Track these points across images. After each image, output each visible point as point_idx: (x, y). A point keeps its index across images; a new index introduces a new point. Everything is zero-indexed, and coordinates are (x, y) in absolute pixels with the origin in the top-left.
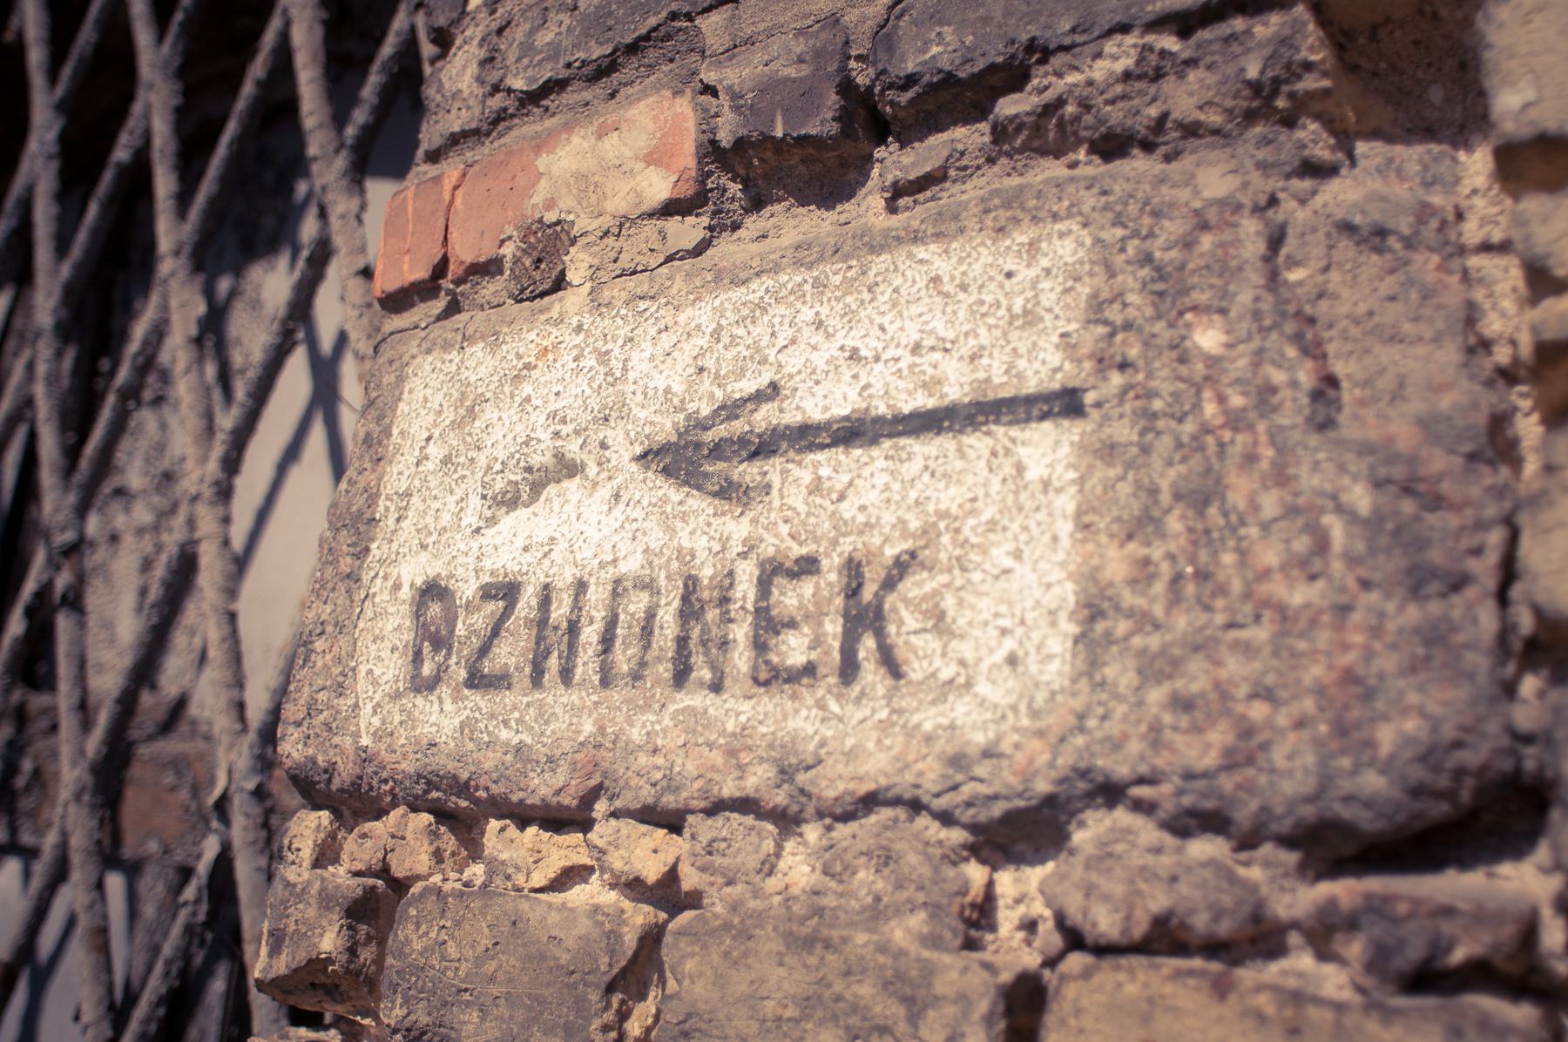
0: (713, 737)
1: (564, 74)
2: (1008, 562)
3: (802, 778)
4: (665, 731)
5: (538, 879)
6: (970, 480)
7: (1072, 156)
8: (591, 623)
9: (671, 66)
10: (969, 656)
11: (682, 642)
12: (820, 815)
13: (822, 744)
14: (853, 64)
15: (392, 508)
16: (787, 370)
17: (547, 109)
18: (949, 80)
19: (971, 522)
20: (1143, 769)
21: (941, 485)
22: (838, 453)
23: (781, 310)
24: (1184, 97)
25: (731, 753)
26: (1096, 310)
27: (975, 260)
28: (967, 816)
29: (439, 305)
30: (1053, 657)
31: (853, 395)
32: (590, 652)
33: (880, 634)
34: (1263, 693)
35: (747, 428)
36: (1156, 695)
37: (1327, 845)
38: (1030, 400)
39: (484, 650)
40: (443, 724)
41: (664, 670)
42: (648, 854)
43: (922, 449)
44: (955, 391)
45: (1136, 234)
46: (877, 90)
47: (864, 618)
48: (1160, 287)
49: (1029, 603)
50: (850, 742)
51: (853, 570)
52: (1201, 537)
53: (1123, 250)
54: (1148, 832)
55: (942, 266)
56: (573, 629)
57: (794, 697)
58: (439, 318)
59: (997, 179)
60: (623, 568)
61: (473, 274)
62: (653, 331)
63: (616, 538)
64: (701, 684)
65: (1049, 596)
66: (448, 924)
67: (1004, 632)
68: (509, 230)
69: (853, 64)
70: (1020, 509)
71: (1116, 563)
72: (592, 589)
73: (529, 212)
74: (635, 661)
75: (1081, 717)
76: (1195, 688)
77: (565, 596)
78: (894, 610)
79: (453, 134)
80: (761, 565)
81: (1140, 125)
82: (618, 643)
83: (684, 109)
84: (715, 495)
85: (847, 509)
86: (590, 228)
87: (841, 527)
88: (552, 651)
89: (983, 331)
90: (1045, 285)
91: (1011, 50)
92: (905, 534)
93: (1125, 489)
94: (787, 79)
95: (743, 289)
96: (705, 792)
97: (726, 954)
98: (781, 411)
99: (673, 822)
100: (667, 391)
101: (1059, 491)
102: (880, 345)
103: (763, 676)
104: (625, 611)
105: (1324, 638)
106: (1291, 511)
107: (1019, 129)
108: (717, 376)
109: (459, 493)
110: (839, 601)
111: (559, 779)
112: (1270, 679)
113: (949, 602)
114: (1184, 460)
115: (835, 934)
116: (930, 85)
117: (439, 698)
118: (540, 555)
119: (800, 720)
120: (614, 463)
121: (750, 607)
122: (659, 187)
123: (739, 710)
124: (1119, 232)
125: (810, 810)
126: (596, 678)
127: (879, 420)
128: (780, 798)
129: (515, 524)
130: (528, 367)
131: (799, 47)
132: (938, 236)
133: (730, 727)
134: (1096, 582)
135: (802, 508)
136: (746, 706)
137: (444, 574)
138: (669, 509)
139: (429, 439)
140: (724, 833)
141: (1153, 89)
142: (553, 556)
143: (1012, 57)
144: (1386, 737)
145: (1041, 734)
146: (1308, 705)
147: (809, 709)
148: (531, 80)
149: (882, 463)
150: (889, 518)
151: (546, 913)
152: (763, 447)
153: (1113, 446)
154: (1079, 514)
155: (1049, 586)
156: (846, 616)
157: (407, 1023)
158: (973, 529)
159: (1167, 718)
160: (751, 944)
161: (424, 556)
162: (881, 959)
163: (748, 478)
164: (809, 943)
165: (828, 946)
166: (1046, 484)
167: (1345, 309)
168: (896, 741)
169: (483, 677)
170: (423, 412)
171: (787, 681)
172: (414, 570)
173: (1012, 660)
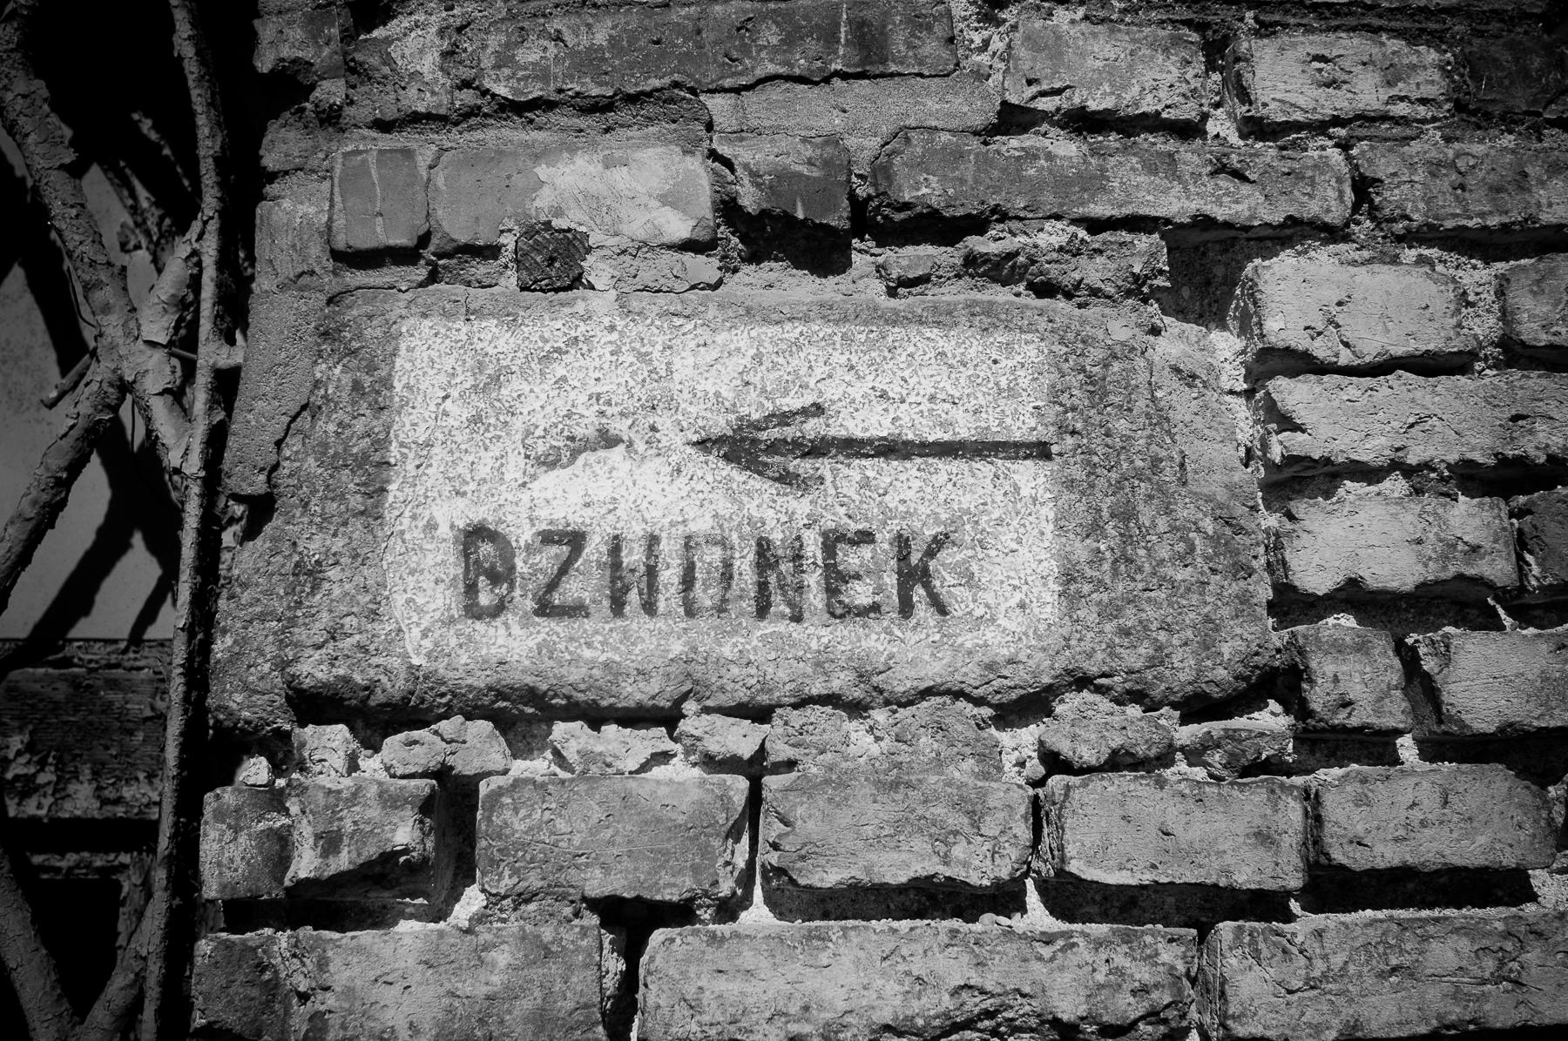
0: (801, 653)
1: (554, 97)
2: (1014, 546)
3: (875, 680)
4: (755, 649)
6: (981, 491)
7: (1016, 289)
9: (674, 126)
10: (991, 602)
11: (763, 586)
13: (891, 657)
14: (854, 179)
15: (411, 455)
17: (531, 121)
18: (935, 214)
19: (985, 518)
20: (1105, 669)
21: (960, 492)
22: (880, 462)
23: (814, 350)
24: (1093, 271)
25: (818, 664)
26: (1055, 395)
27: (966, 344)
28: (996, 699)
29: (421, 272)
30: (1047, 603)
31: (887, 422)
32: (673, 590)
33: (927, 586)
34: (1166, 627)
35: (799, 434)
36: (1109, 627)
37: (1196, 707)
38: (1017, 446)
39: (552, 586)
40: (513, 646)
41: (748, 605)
42: (740, 739)
43: (945, 468)
44: (964, 429)
45: (1074, 352)
46: (874, 204)
47: (913, 575)
48: (1091, 388)
49: (1029, 571)
50: (911, 655)
51: (902, 543)
52: (1126, 538)
53: (1067, 360)
54: (1104, 704)
55: (948, 347)
56: (652, 572)
57: (864, 626)
58: (422, 285)
59: (954, 293)
60: (693, 527)
61: (464, 253)
62: (692, 344)
63: (682, 504)
64: (783, 616)
66: (553, 806)
67: (1015, 588)
68: (510, 224)
69: (854, 179)
70: (1017, 513)
71: (1081, 551)
73: (533, 213)
74: (718, 597)
76: (1129, 624)
77: (636, 546)
79: (415, 113)
80: (825, 534)
81: (1067, 281)
82: (698, 585)
83: (697, 168)
85: (891, 500)
86: (608, 243)
87: (887, 514)
88: (628, 587)
89: (979, 395)
90: (1021, 373)
92: (937, 521)
93: (1081, 507)
94: (800, 175)
96: (793, 693)
97: (830, 800)
99: (760, 714)
100: (717, 395)
101: (1042, 504)
103: (839, 611)
104: (700, 560)
106: (1173, 529)
107: (984, 262)
109: (496, 450)
110: (893, 563)
111: (654, 686)
112: (1169, 620)
113: (975, 568)
114: (1114, 494)
115: (913, 778)
116: (921, 214)
117: (506, 624)
118: (603, 511)
119: (873, 641)
121: (820, 562)
122: (680, 229)
123: (817, 634)
124: (1065, 349)
125: (880, 700)
127: (906, 443)
128: (857, 694)
129: (549, 481)
130: (558, 350)
131: (808, 152)
133: (814, 645)
134: (1070, 561)
135: (856, 498)
136: (824, 632)
137: (490, 519)
138: (735, 486)
139: (446, 397)
140: (812, 719)
142: (618, 512)
143: (982, 213)
144: (1226, 649)
145: (1044, 649)
146: (1189, 633)
148: (515, 91)
149: (914, 472)
150: (924, 510)
151: (642, 787)
152: (817, 449)
153: (1072, 481)
156: (900, 573)
157: (519, 889)
158: (988, 522)
159: (1117, 641)
161: (460, 502)
162: (949, 790)
164: (895, 786)
165: (909, 785)
167: (1179, 417)
169: (554, 607)
170: (431, 372)
171: (857, 615)
172: (453, 514)
173: (1022, 606)
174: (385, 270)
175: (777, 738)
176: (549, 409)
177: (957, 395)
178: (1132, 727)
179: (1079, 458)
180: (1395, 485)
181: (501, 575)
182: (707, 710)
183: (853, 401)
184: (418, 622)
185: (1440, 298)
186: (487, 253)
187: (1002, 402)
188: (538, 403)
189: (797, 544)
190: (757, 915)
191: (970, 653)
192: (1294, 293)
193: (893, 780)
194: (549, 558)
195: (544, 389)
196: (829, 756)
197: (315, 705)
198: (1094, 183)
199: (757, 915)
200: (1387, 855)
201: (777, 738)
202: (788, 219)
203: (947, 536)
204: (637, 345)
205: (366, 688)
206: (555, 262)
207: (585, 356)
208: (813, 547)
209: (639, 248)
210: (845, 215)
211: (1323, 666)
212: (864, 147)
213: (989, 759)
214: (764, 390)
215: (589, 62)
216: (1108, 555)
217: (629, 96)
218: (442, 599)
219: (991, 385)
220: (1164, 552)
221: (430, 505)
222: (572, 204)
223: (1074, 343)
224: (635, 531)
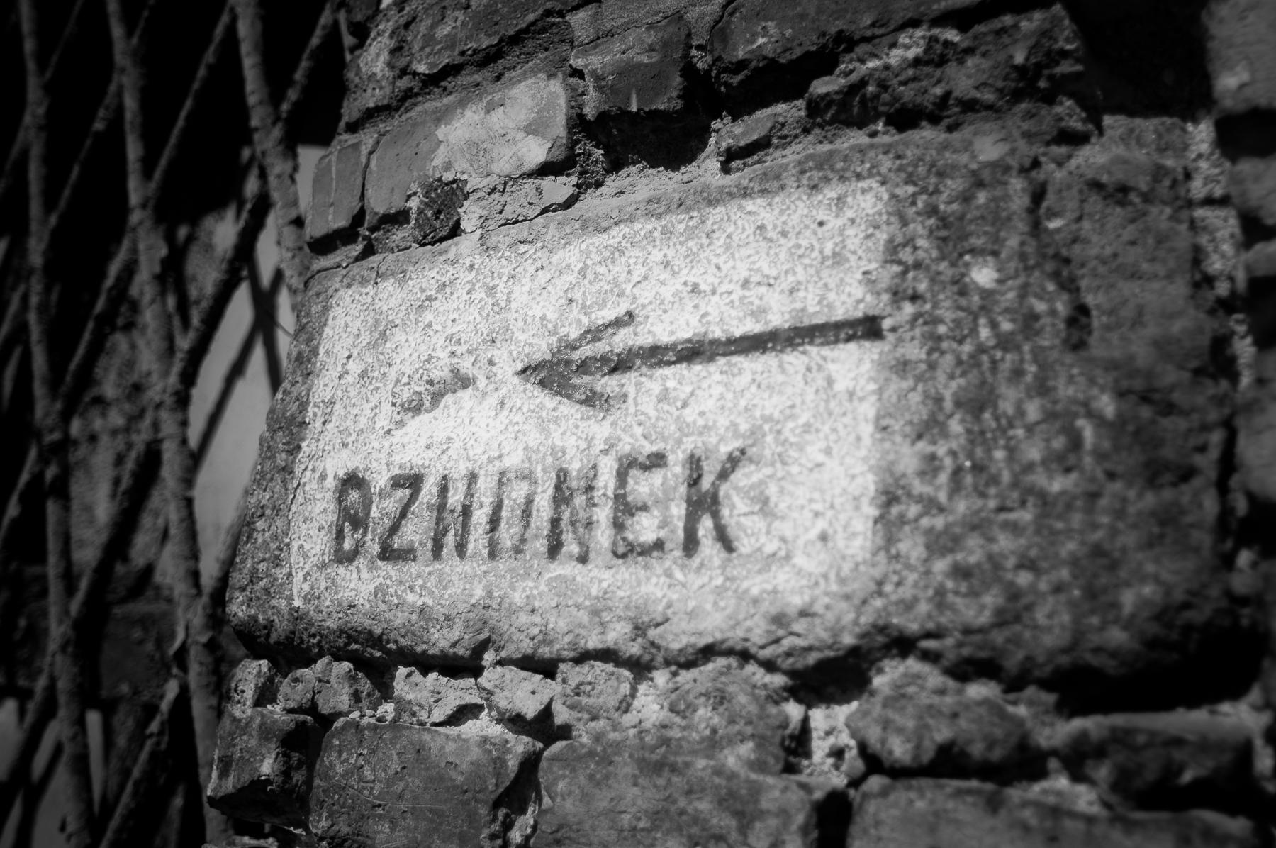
0: (580, 600)
1: (458, 60)
2: (821, 458)
3: (653, 633)
4: (541, 594)
5: (438, 716)
8: (481, 507)
9: (546, 54)
10: (789, 534)
11: (555, 522)
13: (669, 606)
14: (694, 52)
15: (319, 414)
20: (930, 626)
21: (766, 395)
22: (682, 368)
24: (964, 79)
25: (595, 613)
26: (892, 252)
28: (787, 664)
29: (357, 248)
30: (857, 535)
31: (694, 321)
32: (480, 531)
33: (716, 515)
35: (608, 349)
36: (941, 566)
37: (1076, 686)
38: (838, 326)
39: (394, 529)
41: (541, 545)
42: (526, 695)
44: (778, 318)
45: (924, 190)
46: (714, 73)
47: (703, 503)
48: (944, 233)
49: (837, 491)
51: (694, 463)
52: (976, 437)
53: (914, 203)
56: (466, 512)
57: (646, 567)
58: (357, 259)
60: (507, 462)
62: (531, 270)
63: (501, 438)
66: (365, 752)
67: (817, 514)
68: (414, 187)
69: (694, 52)
73: (431, 172)
74: (517, 538)
75: (880, 583)
76: (973, 559)
77: (460, 485)
79: (368, 109)
81: (927, 102)
82: (503, 524)
83: (556, 88)
84: (582, 402)
85: (690, 414)
86: (480, 186)
87: (684, 429)
90: (850, 232)
92: (737, 435)
93: (915, 398)
96: (573, 645)
98: (636, 334)
99: (547, 668)
100: (543, 318)
101: (861, 399)
102: (716, 281)
103: (621, 550)
104: (509, 497)
105: (1077, 519)
106: (1050, 416)
107: (829, 105)
108: (584, 306)
110: (683, 489)
111: (455, 634)
113: (772, 490)
115: (680, 759)
117: (358, 568)
118: (439, 452)
119: (652, 586)
120: (499, 377)
122: (536, 152)
123: (604, 578)
124: (911, 189)
127: (714, 342)
128: (634, 649)
129: (418, 425)
130: (429, 298)
133: (594, 592)
134: (892, 474)
137: (361, 467)
138: (544, 414)
140: (589, 678)
142: (450, 452)
143: (824, 46)
144: (1128, 599)
145: (847, 597)
146: (1065, 574)
147: (658, 576)
149: (717, 377)
150: (723, 422)
152: (621, 364)
154: (878, 418)
155: (853, 477)
156: (689, 501)
157: (331, 833)
158: (792, 430)
159: (950, 584)
162: (717, 780)
163: (609, 390)
164: (659, 767)
165: (674, 769)
166: (851, 394)
167: (1094, 251)
168: (729, 603)
169: (393, 551)
170: (344, 335)
171: (640, 554)
172: (337, 465)
173: (824, 538)
174: (338, 252)
176: (415, 356)
177: (774, 273)
179: (918, 332)
182: (501, 663)
183: (662, 303)
186: (401, 219)
187: (825, 273)
189: (592, 473)
191: (756, 601)
195: (415, 337)
196: (601, 724)
202: (624, 113)
203: (743, 452)
204: (488, 280)
205: (265, 627)
206: (440, 219)
208: (606, 480)
209: (505, 184)
210: (675, 94)
214: (584, 306)
216: (948, 462)
217: (511, 37)
219: (815, 254)
220: (1034, 453)
222: (459, 156)
224: (459, 471)
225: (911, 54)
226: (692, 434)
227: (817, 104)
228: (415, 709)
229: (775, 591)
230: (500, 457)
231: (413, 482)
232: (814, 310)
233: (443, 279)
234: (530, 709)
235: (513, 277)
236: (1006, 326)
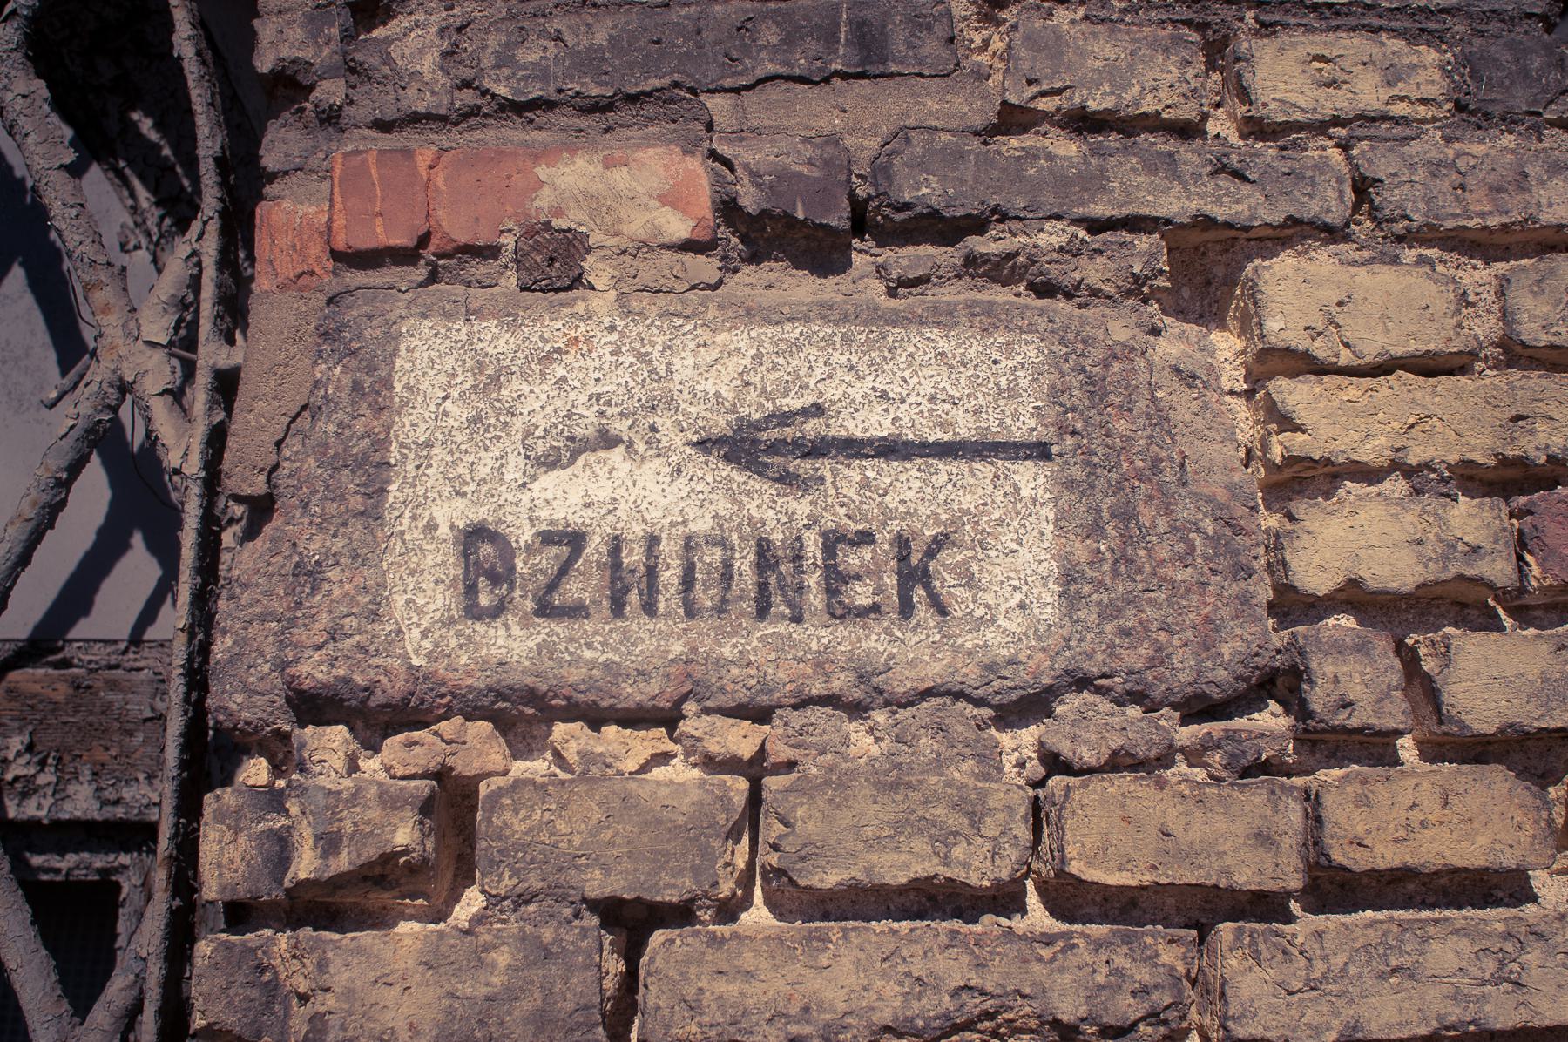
1: (554, 97)
2: (1014, 546)
3: (875, 680)
4: (755, 649)
5: (632, 765)
6: (980, 492)
7: (1016, 289)
8: (668, 568)
9: (673, 126)
10: (991, 602)
11: (763, 587)
12: (887, 704)
14: (854, 179)
15: (411, 456)
16: (828, 396)
17: (531, 121)
18: (935, 214)
23: (814, 350)
24: (1094, 271)
25: (818, 665)
26: (1054, 395)
29: (421, 273)
30: (1048, 605)
31: (887, 423)
32: (672, 591)
33: (928, 587)
34: (1166, 628)
37: (1198, 708)
39: (553, 586)
40: (514, 645)
41: (748, 606)
42: (740, 739)
43: (945, 469)
44: (965, 429)
48: (1091, 388)
49: (1029, 572)
51: (902, 544)
52: (1126, 538)
53: (1067, 361)
54: (1105, 705)
56: (652, 572)
57: (864, 627)
58: (422, 285)
59: (953, 293)
60: (693, 527)
62: (692, 345)
63: (682, 504)
64: (783, 616)
65: (1041, 568)
66: (553, 807)
67: (1015, 588)
69: (854, 179)
70: (1018, 514)
71: (1081, 551)
72: (664, 542)
75: (1067, 640)
76: (1130, 624)
78: (937, 571)
79: (415, 113)
83: (696, 168)
84: (775, 480)
86: (608, 243)
87: (887, 514)
91: (981, 208)
92: (938, 522)
93: (1081, 508)
95: (778, 329)
97: (830, 801)
98: (828, 426)
99: (760, 715)
100: (718, 395)
101: (1042, 505)
102: (905, 393)
103: (839, 612)
104: (700, 560)
105: (1195, 599)
106: (1174, 529)
107: (985, 263)
108: (764, 390)
111: (654, 687)
112: (1169, 620)
113: (975, 568)
114: (1114, 494)
116: (921, 214)
118: (603, 512)
120: (664, 443)
122: (678, 227)
123: (817, 635)
125: (880, 700)
126: (681, 611)
127: (907, 443)
128: (857, 694)
129: (549, 482)
130: (558, 350)
131: (808, 152)
132: (938, 324)
133: (814, 646)
134: (1069, 562)
138: (735, 486)
141: (1074, 260)
142: (618, 513)
144: (1226, 650)
145: (1044, 650)
146: (1189, 633)
147: (879, 634)
149: (914, 473)
152: (818, 449)
153: (1072, 482)
154: (1056, 520)
155: (1040, 562)
156: (899, 573)
157: (518, 890)
158: (988, 522)
160: (849, 792)
163: (801, 471)
164: (894, 786)
165: (909, 786)
166: (1034, 500)
168: (946, 656)
169: (554, 607)
170: (431, 373)
171: (857, 616)
172: (451, 514)
173: (1022, 606)
175: (776, 739)
176: (549, 409)
178: (1131, 727)
180: (1396, 486)
181: (501, 575)
184: (419, 622)
185: (1441, 300)
186: (487, 253)
187: (1002, 402)
188: (537, 403)
190: (757, 915)
191: (970, 653)
192: (1294, 293)
193: (892, 780)
194: (573, 590)
195: (543, 390)
197: (314, 706)
198: (1095, 183)
199: (757, 915)
200: (1387, 856)
201: (776, 739)
203: (947, 536)
204: (638, 346)
206: (555, 264)
207: (587, 356)
209: (639, 248)
211: (1323, 667)
212: (865, 146)
213: (989, 760)
214: (764, 390)
215: (589, 62)
218: (440, 600)
220: (1164, 553)
221: (432, 508)
222: (572, 204)
223: (1072, 343)
225: (1054, 240)
226: (895, 518)
227: (975, 258)
228: (609, 760)
229: (986, 646)
230: (684, 522)
231: (575, 540)
232: (993, 426)
233: (573, 334)
234: (746, 750)
235: (670, 348)
236: (1139, 464)
